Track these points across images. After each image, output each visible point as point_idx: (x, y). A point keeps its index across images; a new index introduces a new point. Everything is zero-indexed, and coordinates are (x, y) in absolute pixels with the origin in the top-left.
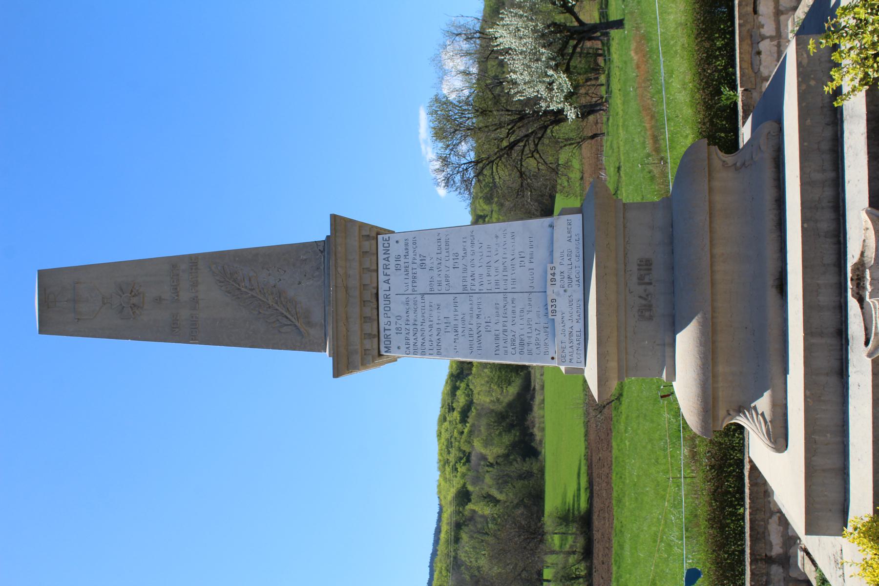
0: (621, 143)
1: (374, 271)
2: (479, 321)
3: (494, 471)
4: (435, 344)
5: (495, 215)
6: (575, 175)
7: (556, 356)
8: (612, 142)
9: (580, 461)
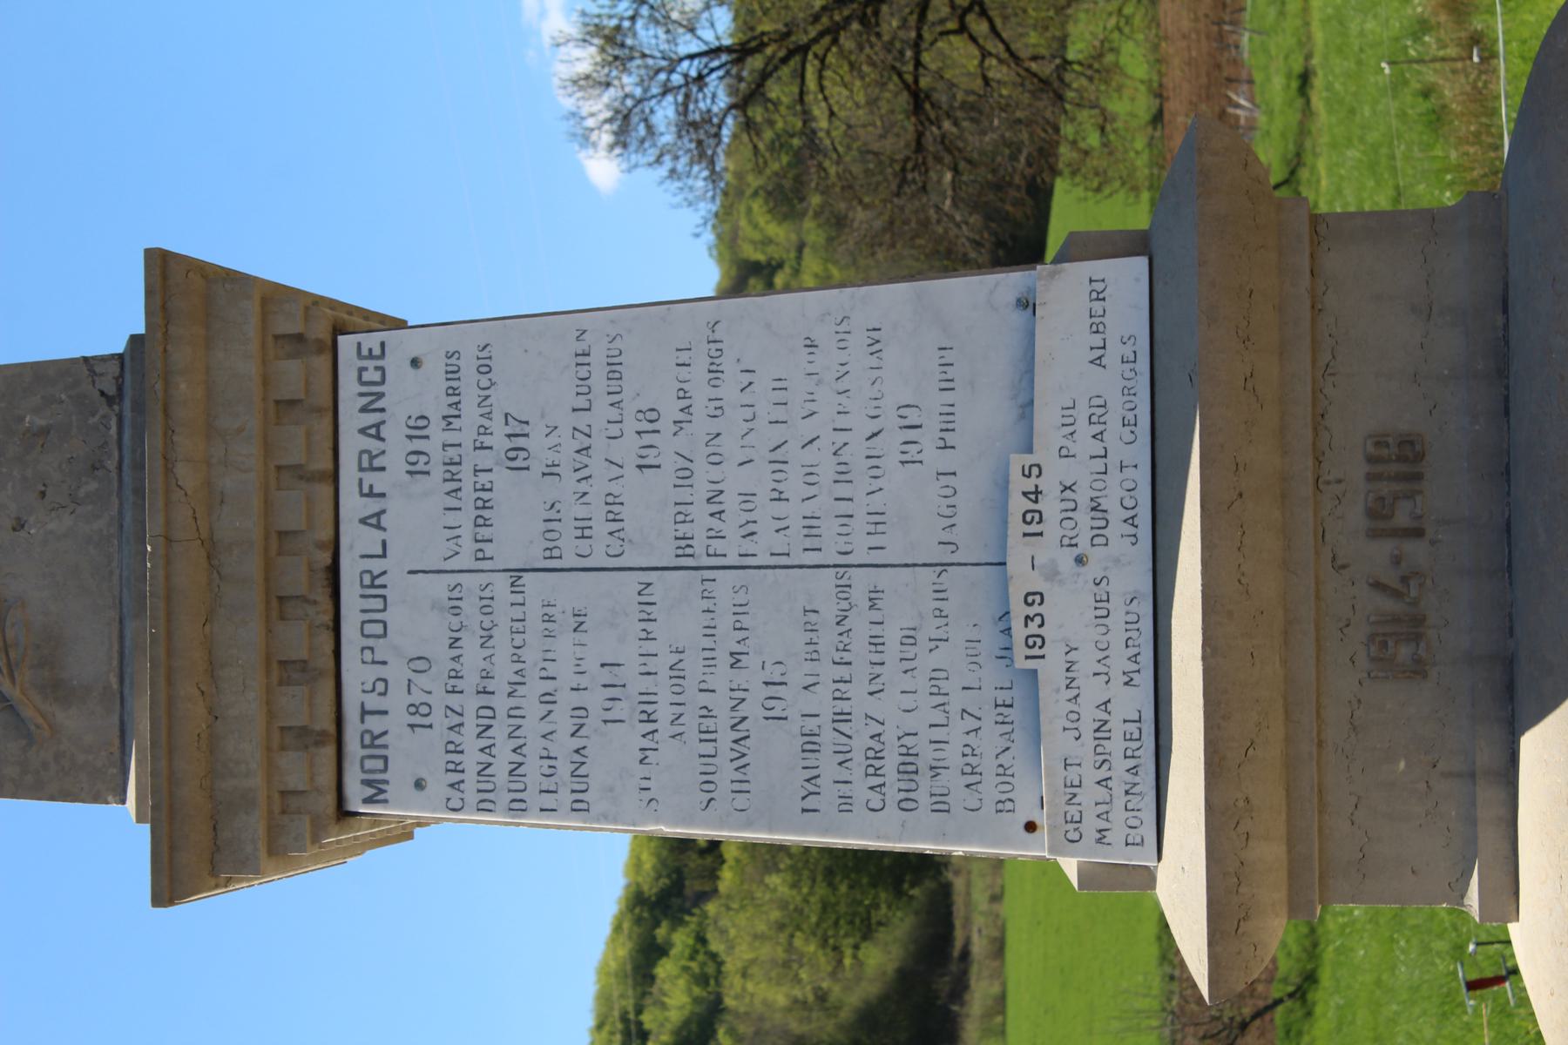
2: (740, 678)
4: (564, 769)
5: (812, 264)
6: (1130, 106)
7: (1042, 820)
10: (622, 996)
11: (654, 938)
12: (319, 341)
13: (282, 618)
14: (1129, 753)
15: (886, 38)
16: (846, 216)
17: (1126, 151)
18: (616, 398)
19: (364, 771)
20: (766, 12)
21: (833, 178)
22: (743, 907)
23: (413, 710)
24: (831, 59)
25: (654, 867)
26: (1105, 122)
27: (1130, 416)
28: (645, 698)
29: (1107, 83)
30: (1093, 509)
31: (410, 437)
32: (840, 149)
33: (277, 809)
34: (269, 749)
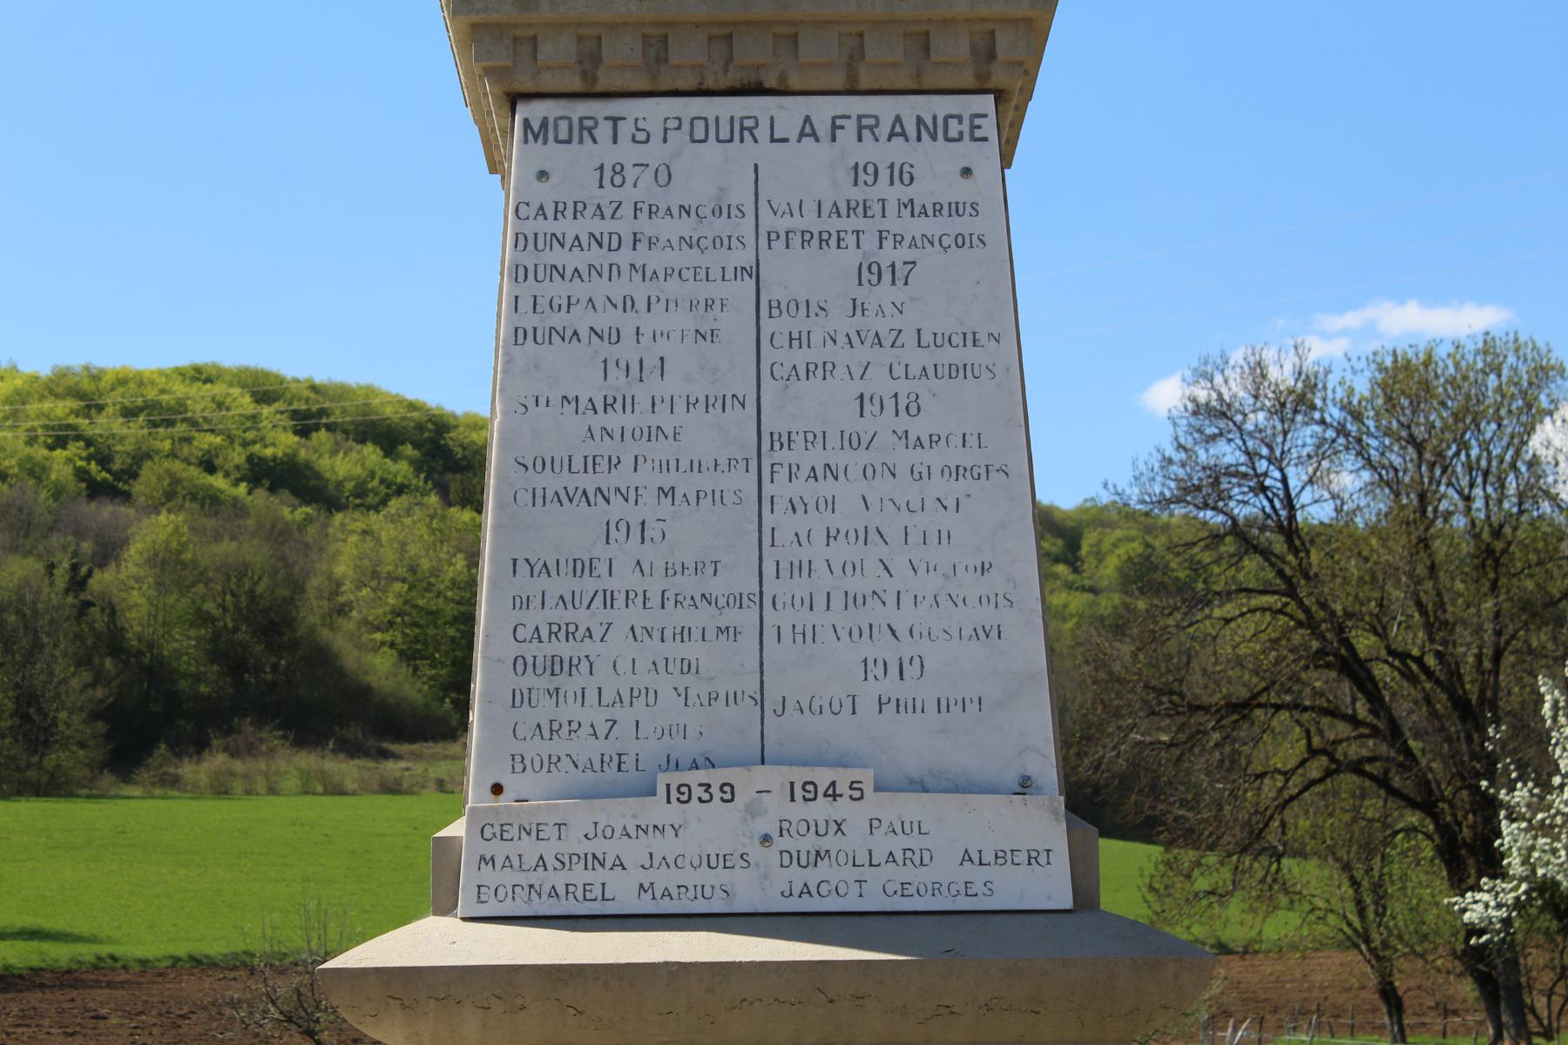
1: (852, 75)
2: (649, 497)
3: (54, 593)
4: (558, 320)
5: (1078, 601)
6: (1236, 921)
7: (504, 801)
9: (92, 940)
10: (344, 411)
11: (403, 443)
12: (988, 75)
13: (711, 38)
14: (571, 889)
15: (1303, 675)
16: (1124, 634)
17: (1189, 916)
18: (931, 372)
19: (556, 119)
20: (1329, 555)
22: (433, 531)
23: (618, 168)
25: (473, 443)
26: (1218, 895)
27: (912, 890)
28: (629, 401)
31: (892, 166)
32: (1191, 630)
33: (519, 33)
34: (579, 24)
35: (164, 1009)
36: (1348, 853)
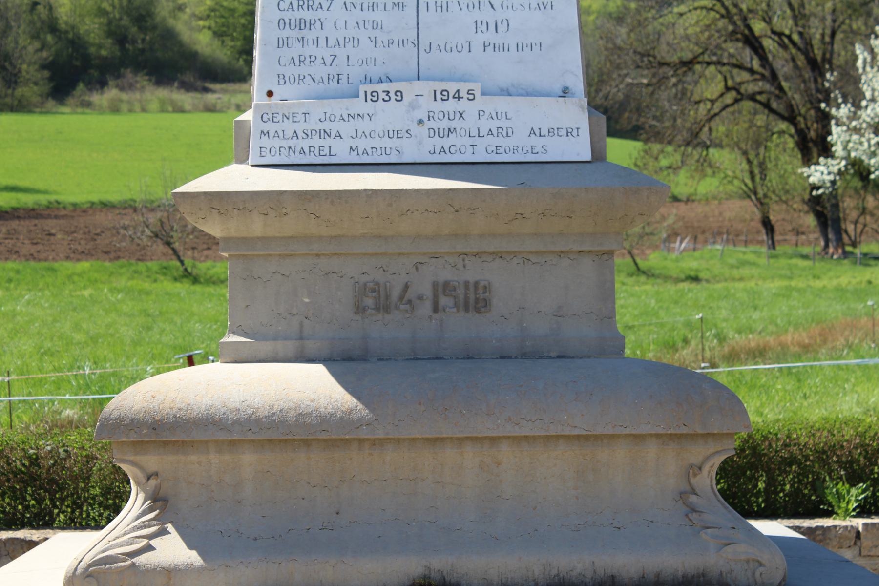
0: (752, 284)
7: (274, 100)
8: (754, 264)
9: (45, 192)
14: (312, 149)
21: (645, 15)
24: (713, 14)
27: (502, 150)
29: (696, 170)
30: (449, 130)
35: (87, 230)
36: (746, 145)
